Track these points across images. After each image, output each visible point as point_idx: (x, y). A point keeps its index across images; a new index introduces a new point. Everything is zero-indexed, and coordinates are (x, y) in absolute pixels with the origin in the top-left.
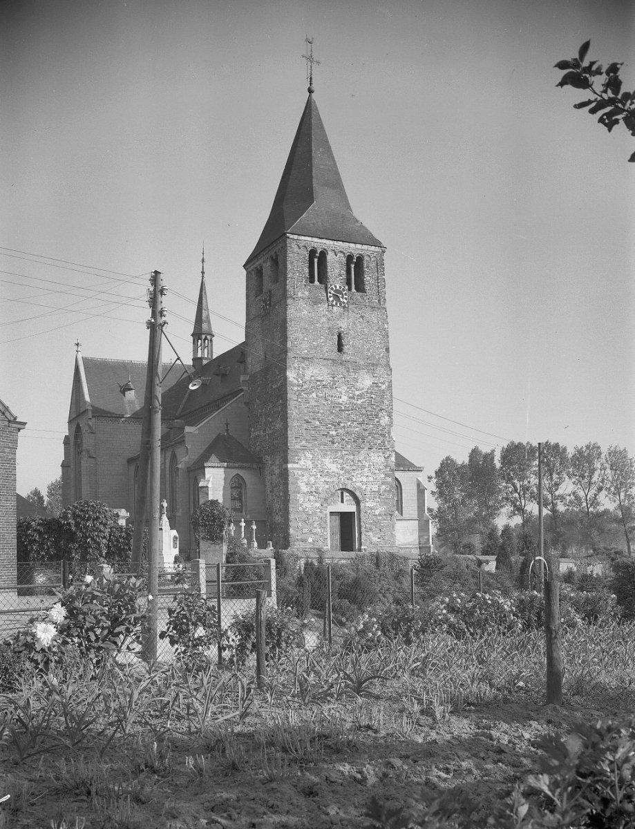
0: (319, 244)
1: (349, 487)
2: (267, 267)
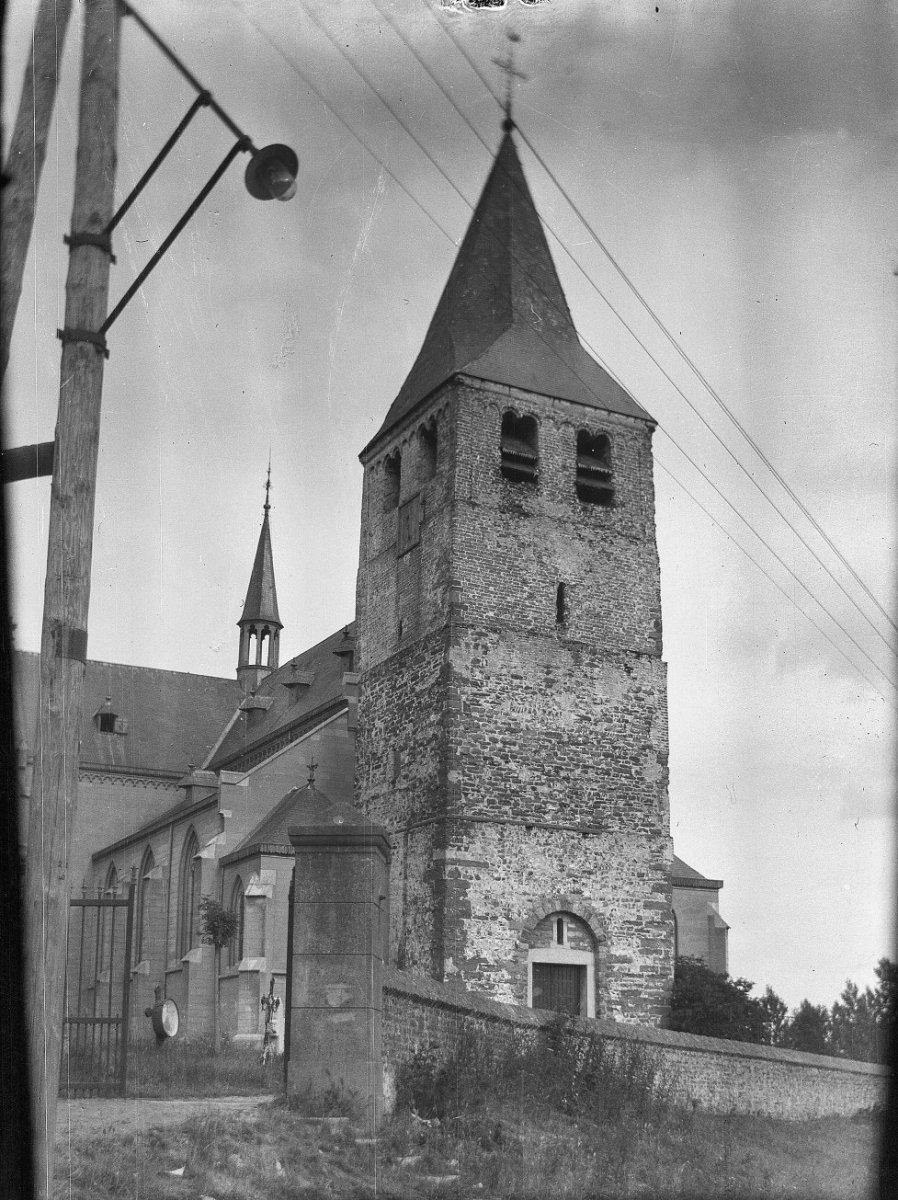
0: (524, 405)
1: (576, 909)
2: (412, 451)
